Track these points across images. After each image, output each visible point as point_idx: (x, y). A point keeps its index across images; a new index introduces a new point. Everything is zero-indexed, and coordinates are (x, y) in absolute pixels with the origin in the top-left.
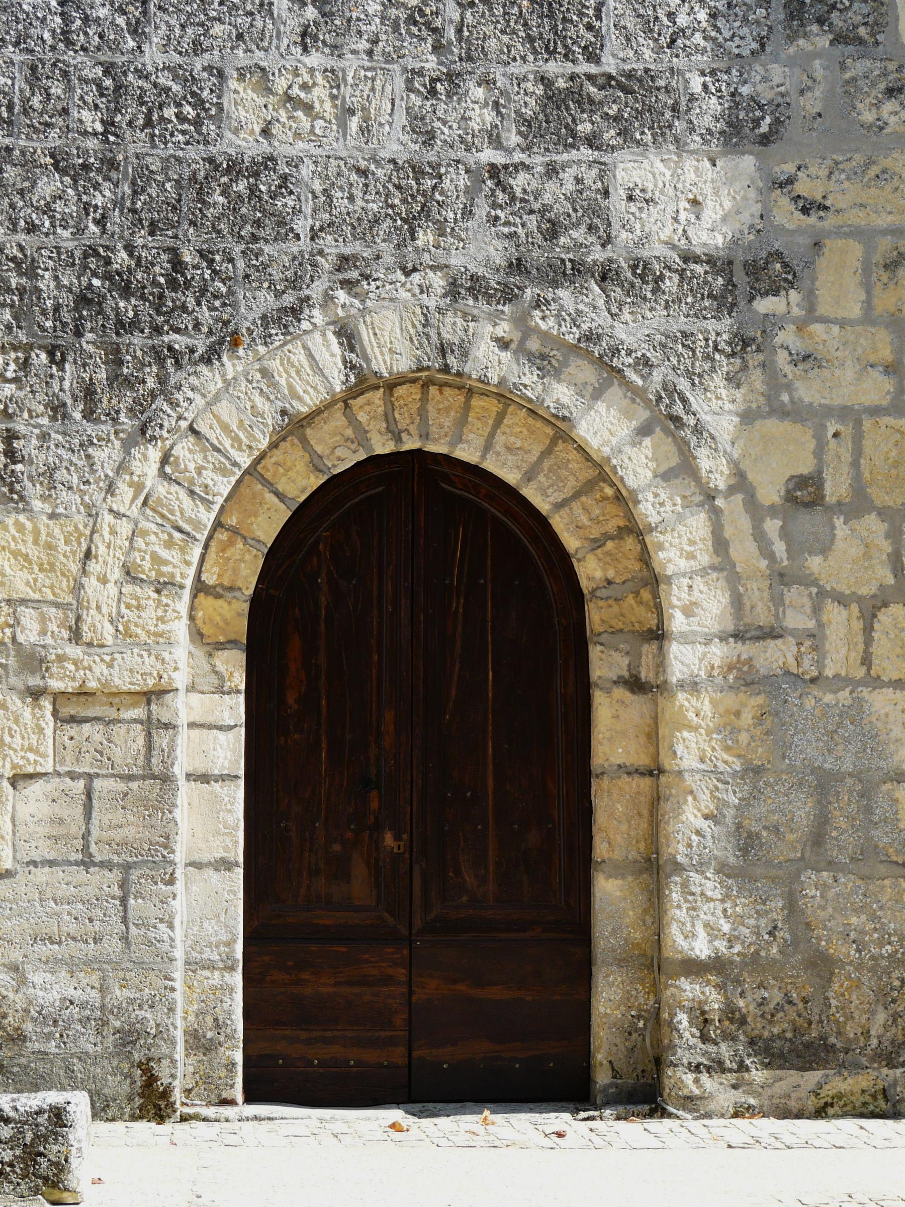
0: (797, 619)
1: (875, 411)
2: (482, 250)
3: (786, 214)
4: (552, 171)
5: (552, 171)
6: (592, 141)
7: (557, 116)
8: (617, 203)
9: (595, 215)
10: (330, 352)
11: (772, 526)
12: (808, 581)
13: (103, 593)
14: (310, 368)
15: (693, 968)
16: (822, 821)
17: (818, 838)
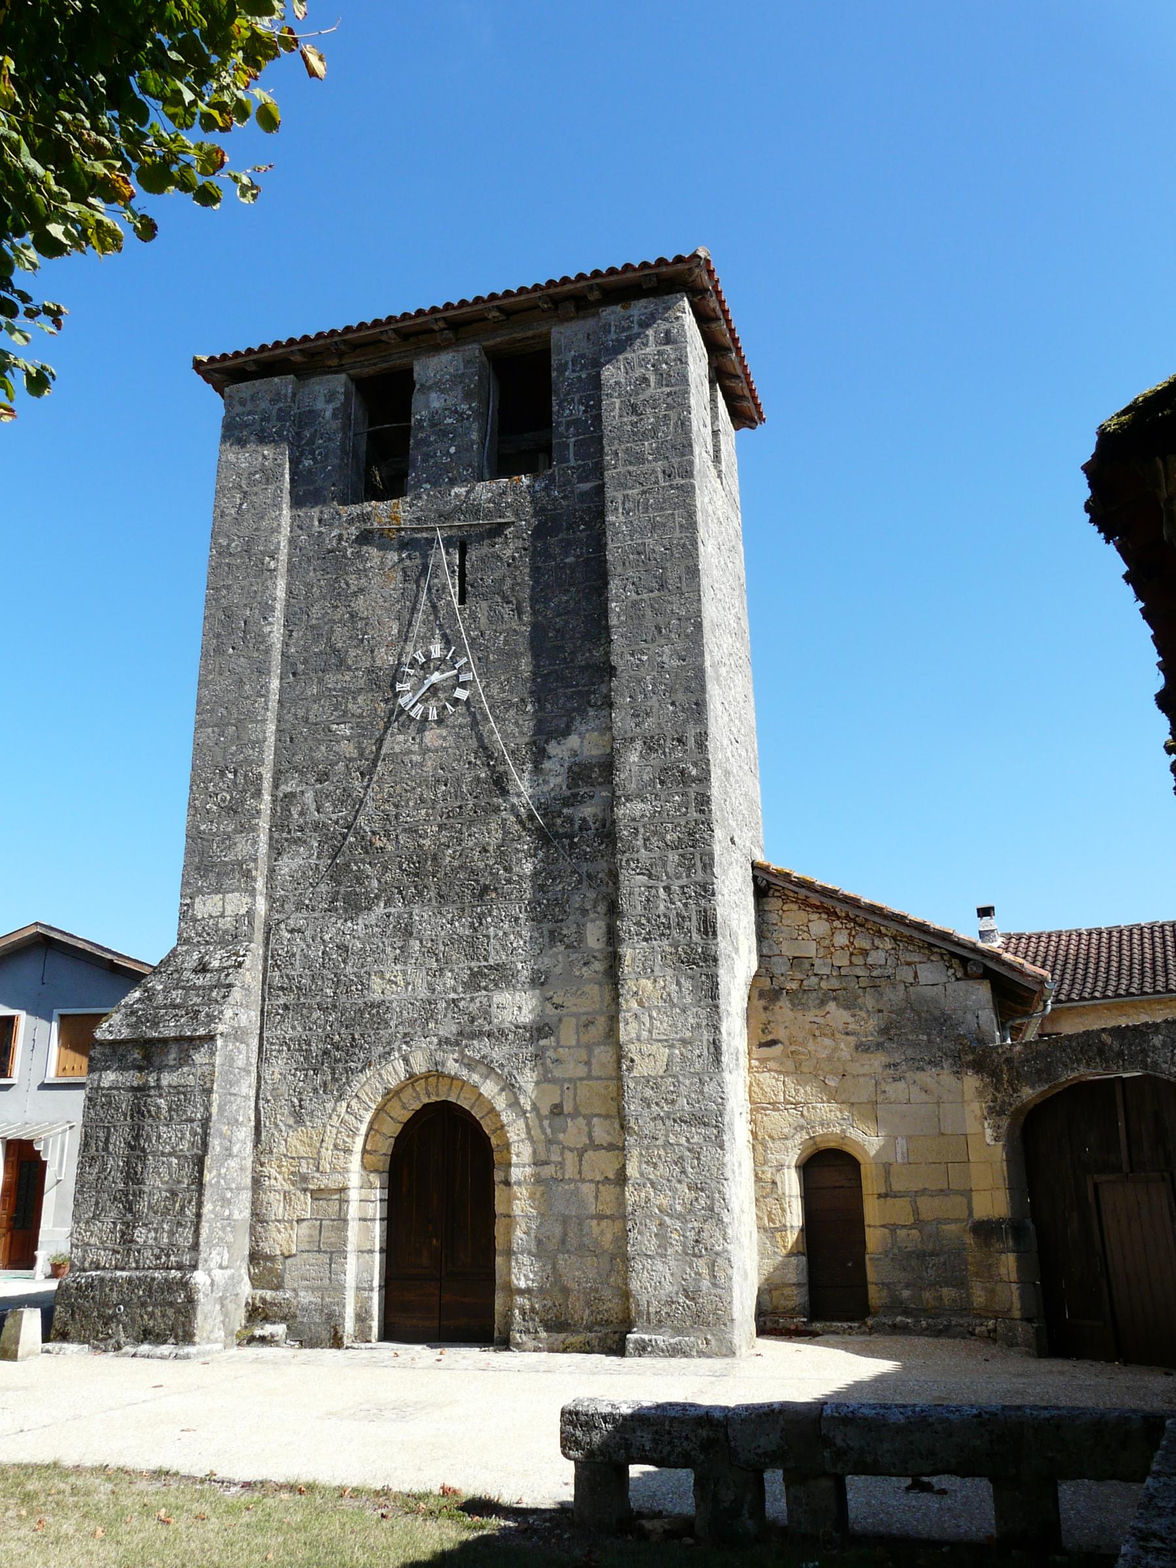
0: (555, 1158)
1: (581, 1079)
2: (449, 1029)
3: (550, 1010)
4: (472, 999)
5: (472, 999)
6: (486, 988)
7: (474, 981)
8: (494, 1009)
9: (486, 1014)
10: (400, 1066)
11: (546, 1123)
12: (559, 1143)
13: (327, 1154)
14: (394, 1073)
15: (521, 1292)
16: (565, 1234)
17: (563, 1242)
